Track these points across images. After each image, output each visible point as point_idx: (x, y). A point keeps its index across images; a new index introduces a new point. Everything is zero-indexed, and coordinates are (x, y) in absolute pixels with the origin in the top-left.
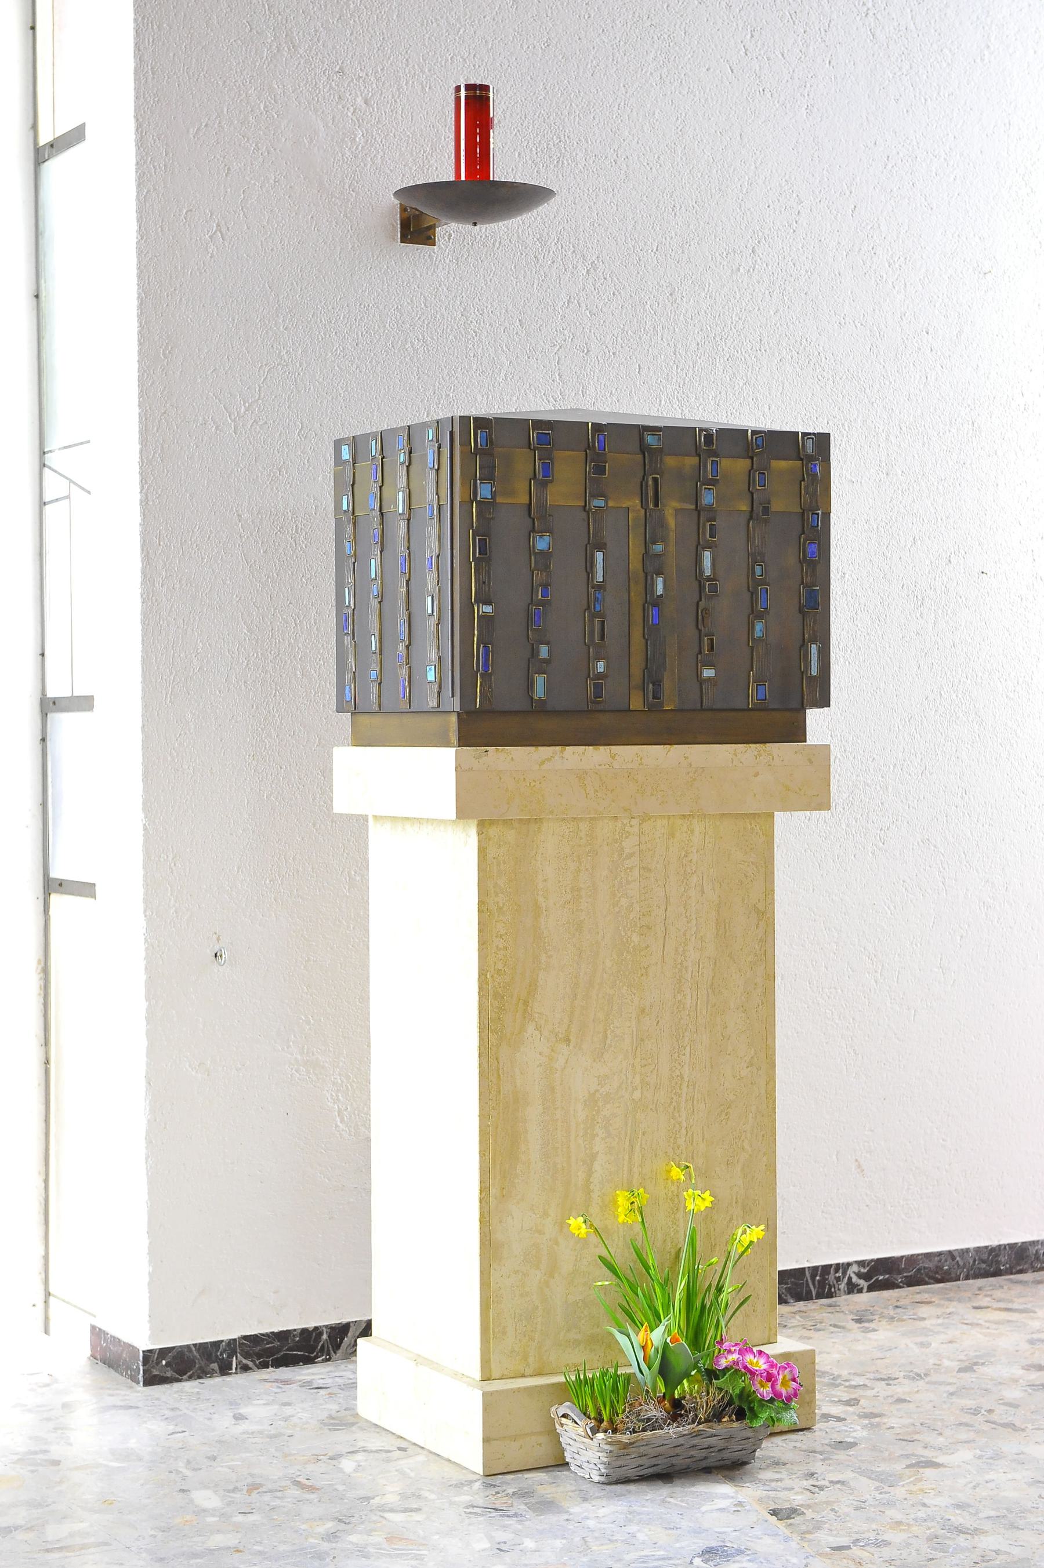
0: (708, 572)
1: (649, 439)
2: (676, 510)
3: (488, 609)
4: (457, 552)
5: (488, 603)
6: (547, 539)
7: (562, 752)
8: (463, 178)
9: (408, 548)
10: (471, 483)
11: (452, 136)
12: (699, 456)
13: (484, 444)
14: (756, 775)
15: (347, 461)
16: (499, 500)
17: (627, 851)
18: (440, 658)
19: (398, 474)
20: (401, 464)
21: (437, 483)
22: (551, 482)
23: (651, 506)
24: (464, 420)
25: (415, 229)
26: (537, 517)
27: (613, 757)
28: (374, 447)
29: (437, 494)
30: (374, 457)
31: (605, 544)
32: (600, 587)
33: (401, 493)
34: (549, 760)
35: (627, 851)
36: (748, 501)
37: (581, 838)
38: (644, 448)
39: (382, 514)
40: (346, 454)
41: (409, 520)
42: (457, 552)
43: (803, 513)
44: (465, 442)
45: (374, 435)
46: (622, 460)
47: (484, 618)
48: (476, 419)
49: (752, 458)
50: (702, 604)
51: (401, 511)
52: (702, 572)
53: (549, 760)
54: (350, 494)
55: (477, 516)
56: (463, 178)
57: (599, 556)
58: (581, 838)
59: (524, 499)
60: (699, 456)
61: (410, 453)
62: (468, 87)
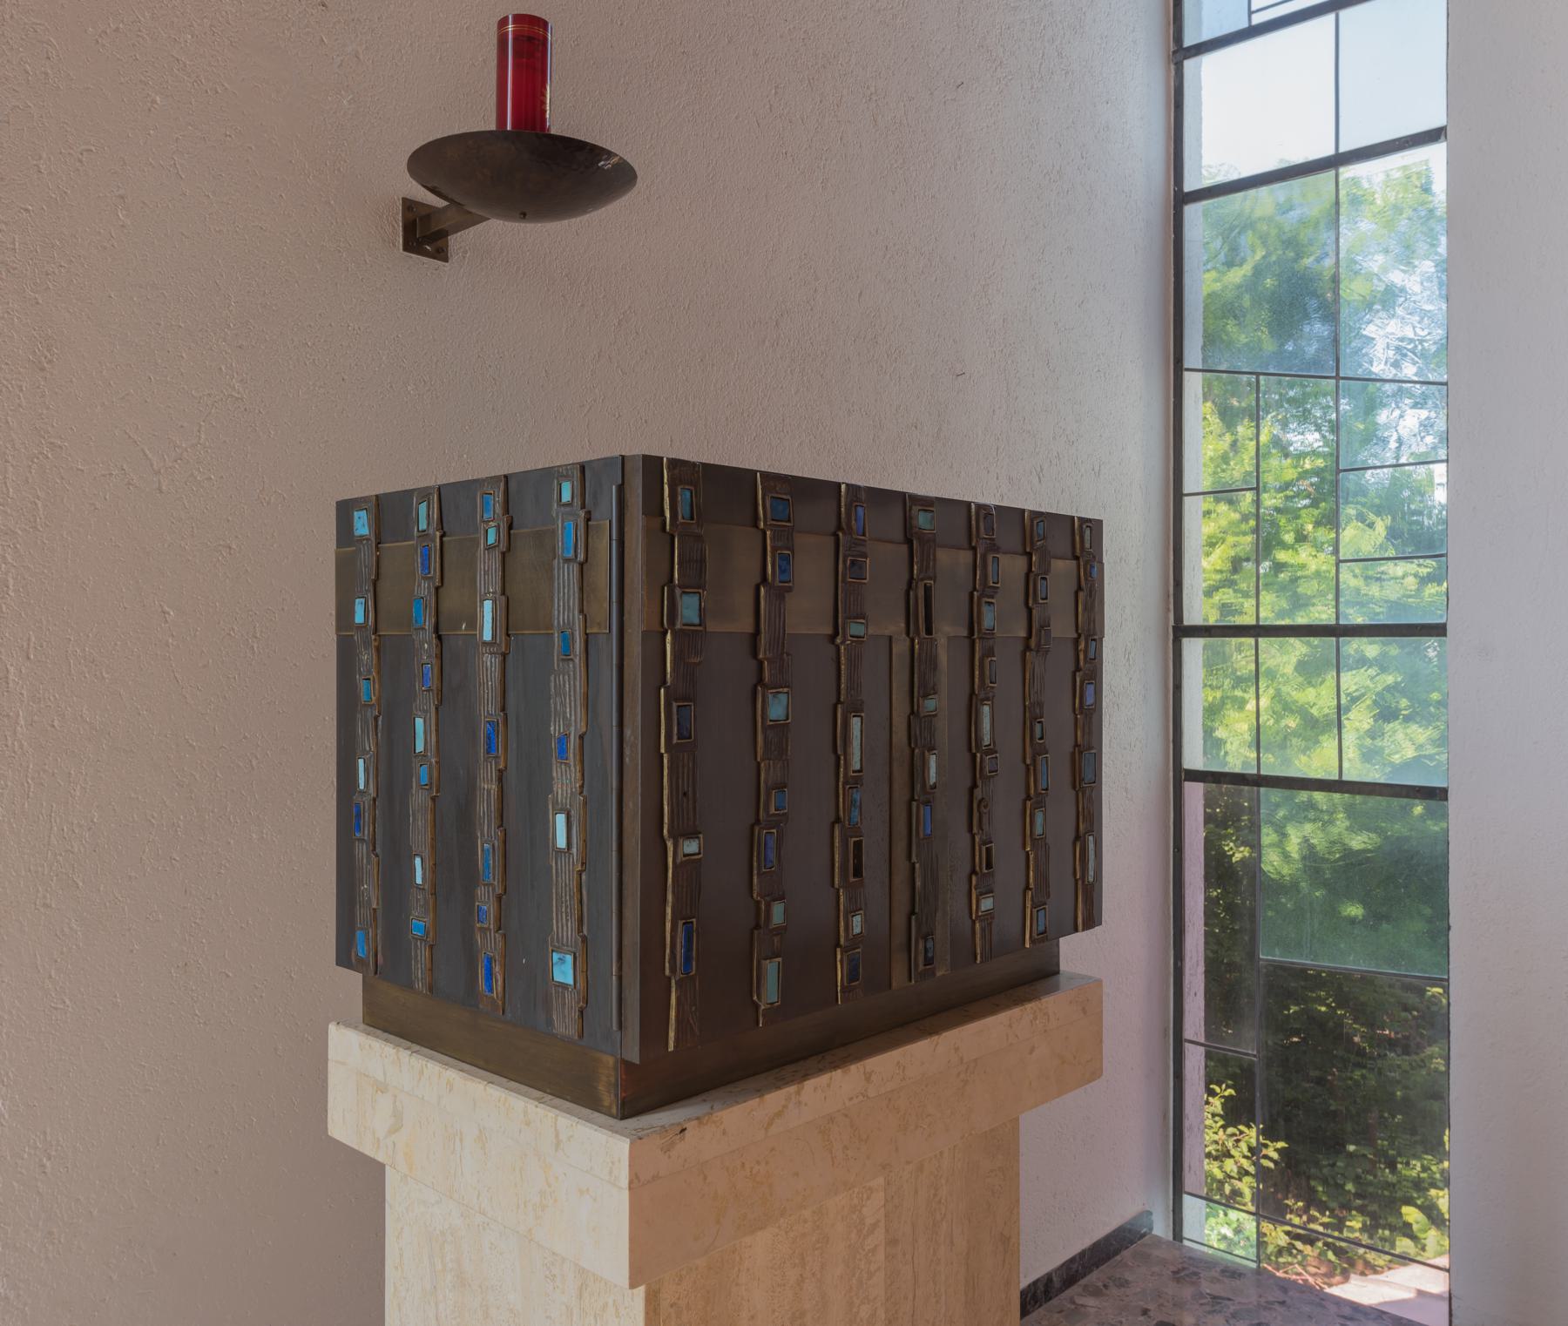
0: (987, 740)
1: (922, 520)
2: (949, 638)
3: (691, 847)
4: (633, 733)
5: (692, 834)
6: (783, 698)
7: (798, 1093)
8: (509, 128)
9: (503, 709)
10: (664, 589)
11: (493, 63)
12: (974, 549)
13: (687, 514)
14: (1032, 1051)
15: (362, 538)
16: (712, 626)
17: (869, 1221)
18: (584, 940)
19: (481, 566)
20: (489, 548)
21: (581, 589)
22: (790, 590)
23: (923, 634)
24: (652, 464)
25: (423, 235)
26: (765, 656)
27: (868, 1079)
28: (423, 516)
29: (581, 611)
30: (424, 535)
31: (863, 702)
32: (856, 781)
33: (488, 605)
34: (779, 1114)
35: (869, 1221)
36: (1023, 623)
37: (805, 1221)
38: (910, 536)
39: (439, 638)
40: (362, 525)
41: (504, 656)
42: (633, 733)
43: (1076, 641)
44: (653, 507)
45: (424, 494)
46: (885, 561)
47: (689, 866)
48: (674, 463)
49: (1030, 555)
50: (978, 793)
51: (487, 636)
52: (979, 740)
53: (779, 1114)
54: (370, 596)
55: (673, 669)
56: (509, 128)
57: (856, 723)
58: (805, 1221)
59: (746, 626)
60: (974, 549)
61: (510, 527)
62: (519, 19)
